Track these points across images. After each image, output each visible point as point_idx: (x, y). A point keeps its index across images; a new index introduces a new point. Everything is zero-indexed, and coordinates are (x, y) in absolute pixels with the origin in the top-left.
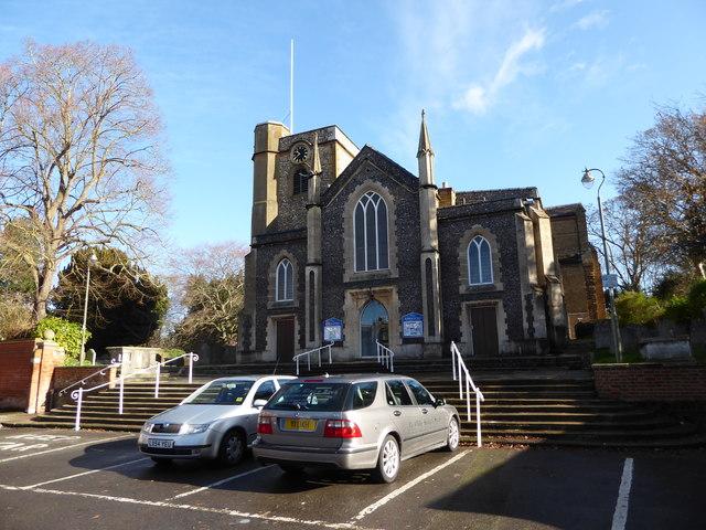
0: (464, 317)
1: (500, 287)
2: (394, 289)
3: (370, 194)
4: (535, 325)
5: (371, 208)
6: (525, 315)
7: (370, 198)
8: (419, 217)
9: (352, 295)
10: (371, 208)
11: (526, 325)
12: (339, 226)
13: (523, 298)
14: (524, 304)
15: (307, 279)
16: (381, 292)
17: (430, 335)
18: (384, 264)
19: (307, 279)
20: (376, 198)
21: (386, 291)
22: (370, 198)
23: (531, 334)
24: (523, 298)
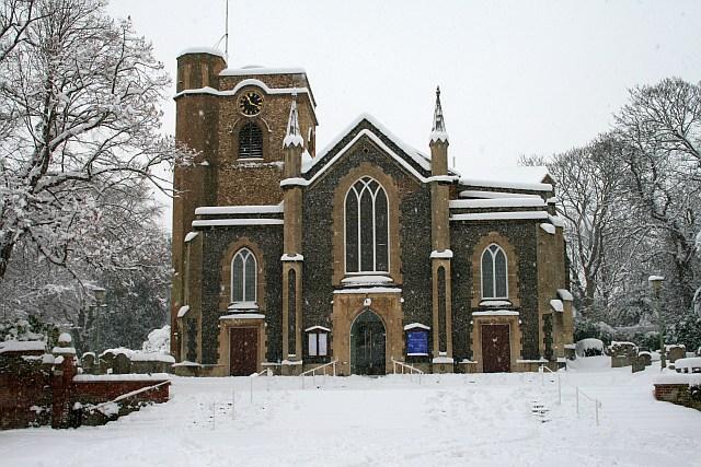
5: (366, 196)
6: (542, 335)
7: (366, 185)
8: (429, 216)
10: (366, 196)
13: (540, 318)
14: (542, 324)
15: (286, 279)
22: (366, 185)
24: (540, 318)
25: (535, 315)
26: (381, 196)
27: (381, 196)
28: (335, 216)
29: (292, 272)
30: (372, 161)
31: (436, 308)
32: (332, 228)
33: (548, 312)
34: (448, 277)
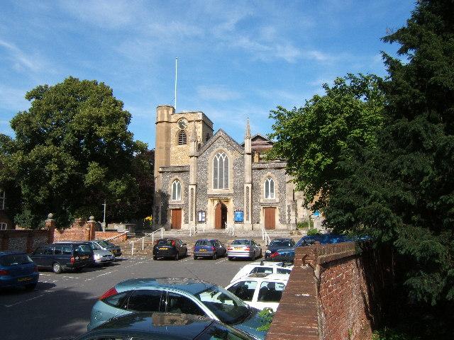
5: (221, 159)
6: (287, 213)
7: (221, 155)
10: (221, 159)
14: (287, 208)
18: (227, 186)
20: (224, 155)
22: (221, 155)
26: (227, 159)
27: (227, 159)
34: (250, 191)
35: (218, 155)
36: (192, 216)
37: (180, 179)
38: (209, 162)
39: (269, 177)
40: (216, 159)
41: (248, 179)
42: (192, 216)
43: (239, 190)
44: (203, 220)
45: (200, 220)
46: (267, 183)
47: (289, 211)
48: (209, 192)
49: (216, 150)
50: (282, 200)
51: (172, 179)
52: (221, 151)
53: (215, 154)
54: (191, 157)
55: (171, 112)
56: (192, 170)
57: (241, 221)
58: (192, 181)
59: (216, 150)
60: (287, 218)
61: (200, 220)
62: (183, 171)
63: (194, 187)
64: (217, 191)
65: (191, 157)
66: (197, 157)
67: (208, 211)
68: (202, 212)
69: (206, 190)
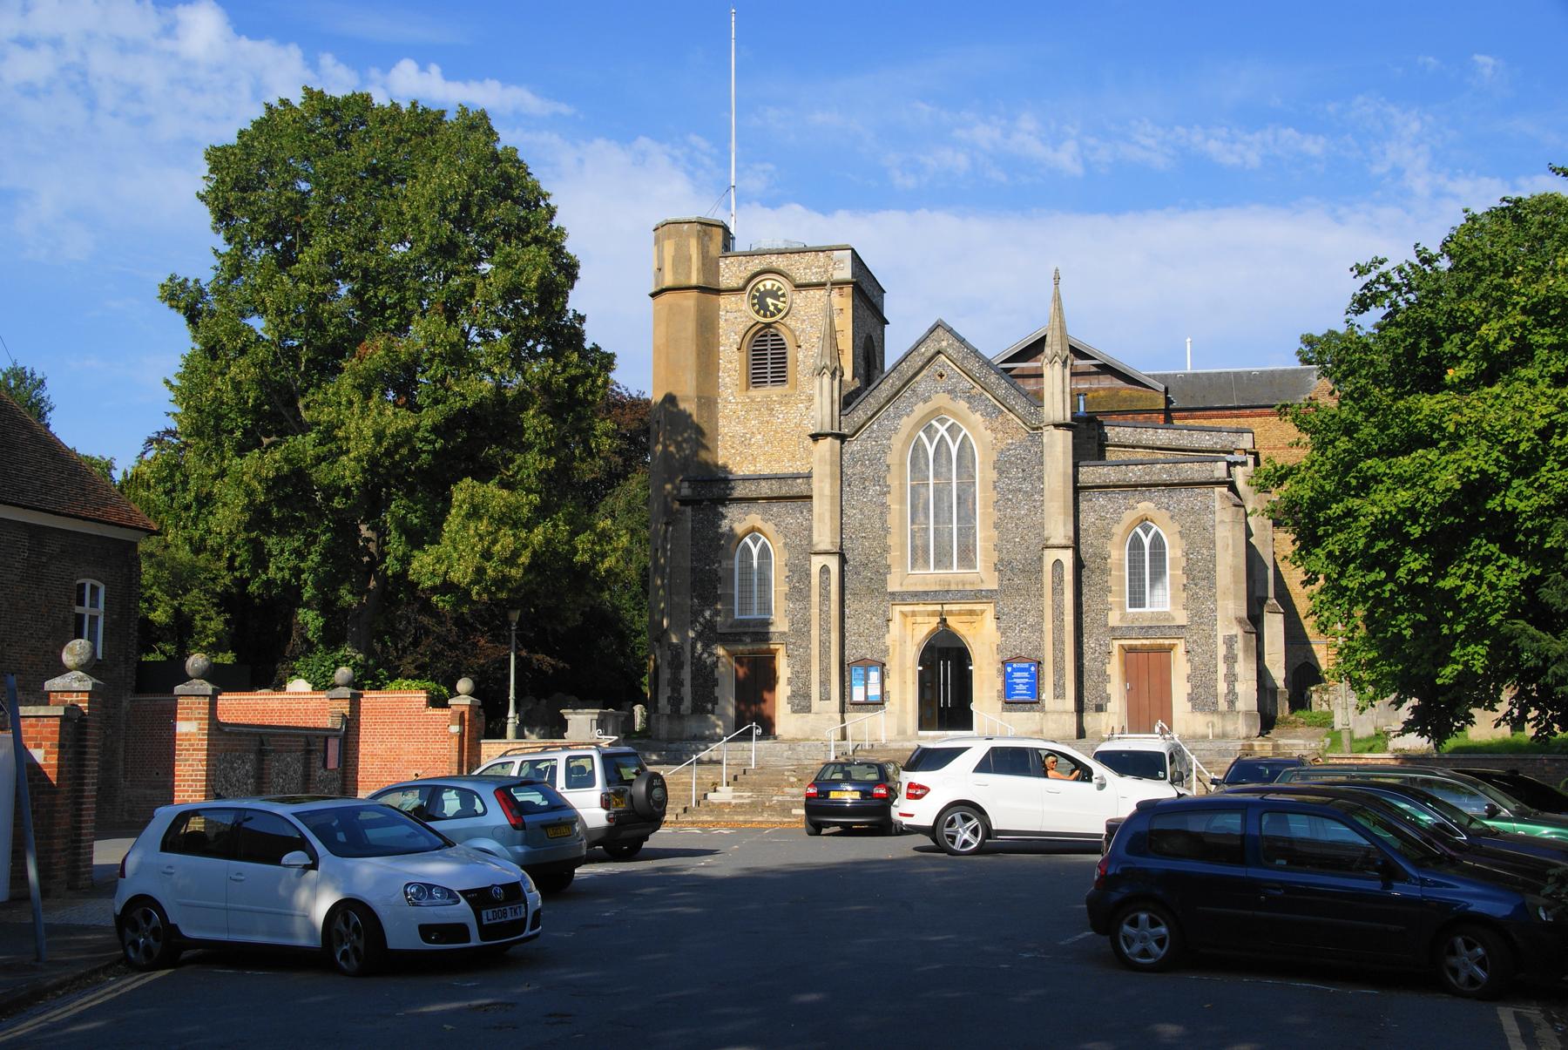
0: (1114, 668)
1: (1181, 618)
2: (990, 610)
3: (942, 421)
4: (1240, 688)
6: (1222, 669)
7: (942, 430)
8: (1041, 479)
9: (904, 615)
11: (1222, 687)
12: (879, 480)
13: (1220, 640)
14: (1222, 650)
15: (815, 580)
16: (960, 613)
17: (1056, 697)
18: (967, 557)
19: (815, 580)
21: (971, 613)
22: (942, 430)
23: (1231, 703)
24: (1220, 640)
25: (1211, 637)
28: (894, 482)
29: (1059, 694)
30: (949, 392)
31: (1048, 626)
32: (888, 499)
33: (1233, 632)
34: (1068, 577)
35: (929, 430)
36: (825, 683)
37: (768, 527)
38: (892, 458)
39: (1144, 522)
40: (918, 449)
41: (1059, 530)
42: (825, 683)
43: (1020, 572)
44: (874, 691)
45: (858, 694)
46: (1136, 544)
47: (1231, 659)
48: (893, 585)
49: (920, 409)
50: (1202, 619)
51: (1128, 517)
52: (937, 413)
53: (917, 426)
54: (815, 437)
55: (715, 247)
56: (823, 489)
57: (1033, 702)
58: (824, 536)
59: (920, 409)
60: (1222, 687)
61: (858, 694)
62: (791, 495)
63: (833, 563)
64: (928, 576)
65: (815, 437)
66: (842, 438)
67: (893, 665)
68: (866, 664)
69: (882, 572)
